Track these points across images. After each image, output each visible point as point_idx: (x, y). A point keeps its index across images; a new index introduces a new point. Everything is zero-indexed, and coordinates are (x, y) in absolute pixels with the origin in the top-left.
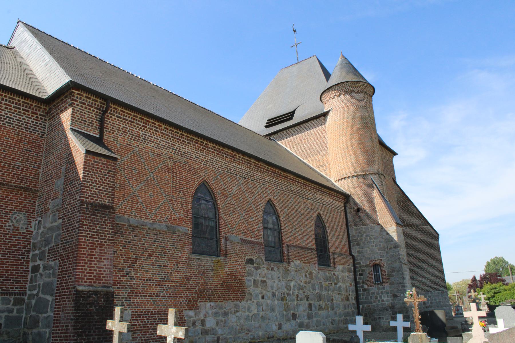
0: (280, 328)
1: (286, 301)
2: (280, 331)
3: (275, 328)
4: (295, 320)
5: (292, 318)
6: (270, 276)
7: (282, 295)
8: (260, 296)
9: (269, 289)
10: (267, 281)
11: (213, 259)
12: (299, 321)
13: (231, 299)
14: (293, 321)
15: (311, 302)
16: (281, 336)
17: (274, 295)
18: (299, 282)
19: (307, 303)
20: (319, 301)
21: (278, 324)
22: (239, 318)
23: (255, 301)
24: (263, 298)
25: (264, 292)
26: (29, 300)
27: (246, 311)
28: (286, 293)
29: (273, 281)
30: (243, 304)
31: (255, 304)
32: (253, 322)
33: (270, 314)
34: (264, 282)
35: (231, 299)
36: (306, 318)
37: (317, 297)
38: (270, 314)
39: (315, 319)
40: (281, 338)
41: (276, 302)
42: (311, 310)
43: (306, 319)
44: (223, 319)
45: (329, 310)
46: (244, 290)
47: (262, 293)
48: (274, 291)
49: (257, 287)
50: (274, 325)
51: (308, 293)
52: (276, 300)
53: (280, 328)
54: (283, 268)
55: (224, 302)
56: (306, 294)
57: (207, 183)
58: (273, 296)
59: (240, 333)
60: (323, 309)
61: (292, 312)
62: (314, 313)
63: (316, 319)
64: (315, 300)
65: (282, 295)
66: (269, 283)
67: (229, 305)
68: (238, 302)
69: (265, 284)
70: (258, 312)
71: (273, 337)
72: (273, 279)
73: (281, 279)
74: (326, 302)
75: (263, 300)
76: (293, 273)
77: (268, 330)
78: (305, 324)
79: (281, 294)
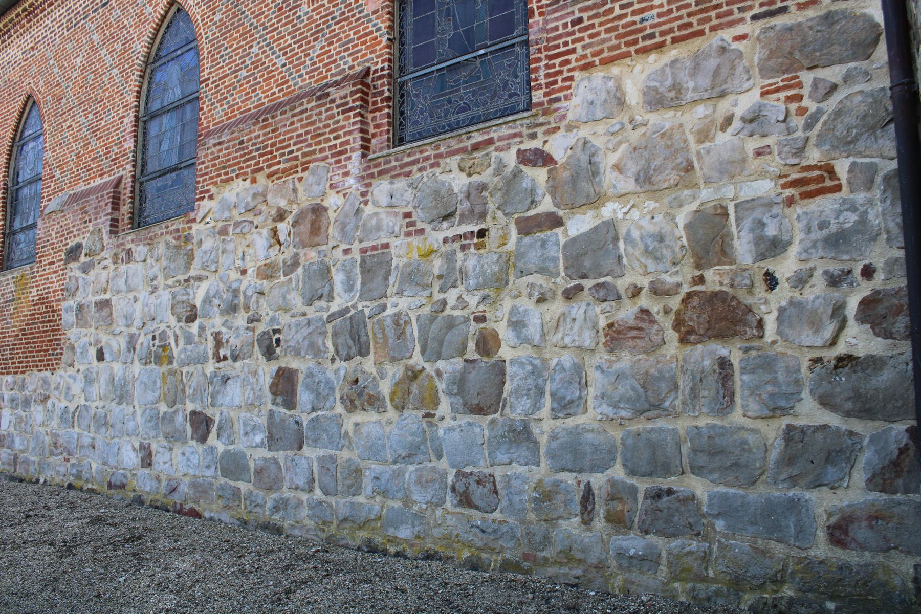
0: (147, 460)
1: (171, 363)
2: (146, 471)
3: (130, 458)
4: (203, 439)
5: (189, 430)
6: (121, 283)
7: (157, 342)
8: (93, 352)
9: (120, 325)
10: (114, 300)
11: (15, 275)
12: (221, 448)
13: (37, 366)
14: (194, 443)
15: (294, 364)
16: (148, 489)
17: (132, 346)
18: (234, 275)
19: (267, 371)
20: (348, 358)
21: (142, 446)
22: (49, 413)
23: (82, 368)
24: (100, 356)
25: (104, 338)
26: (495, 365)
27: (62, 397)
28: (170, 333)
29: (131, 296)
30: (61, 376)
31: (80, 376)
32: (76, 427)
33: (117, 410)
34: (107, 303)
35: (37, 366)
36: (259, 438)
37: (335, 335)
38: (117, 410)
39: (310, 453)
40: (148, 499)
41: (137, 368)
42: (290, 404)
43: (261, 445)
44: (24, 414)
45: (444, 407)
46: (59, 340)
47: (98, 341)
48: (133, 330)
49: (86, 325)
50: (129, 447)
51: (273, 320)
52: (136, 362)
53: (147, 460)
54: (169, 238)
55: (27, 373)
56: (261, 328)
57: (149, 53)
58: (129, 351)
59: (52, 454)
60: (374, 402)
61: (190, 407)
62: (305, 420)
63: (321, 452)
64: (317, 352)
65: (157, 342)
66: (120, 305)
67: (33, 379)
68: (48, 373)
69: (105, 313)
70: (86, 400)
71: (123, 486)
72: (130, 290)
73: (160, 281)
74: (417, 359)
75: (102, 365)
76: (208, 244)
77: (112, 461)
78: (252, 465)
79: (154, 338)
